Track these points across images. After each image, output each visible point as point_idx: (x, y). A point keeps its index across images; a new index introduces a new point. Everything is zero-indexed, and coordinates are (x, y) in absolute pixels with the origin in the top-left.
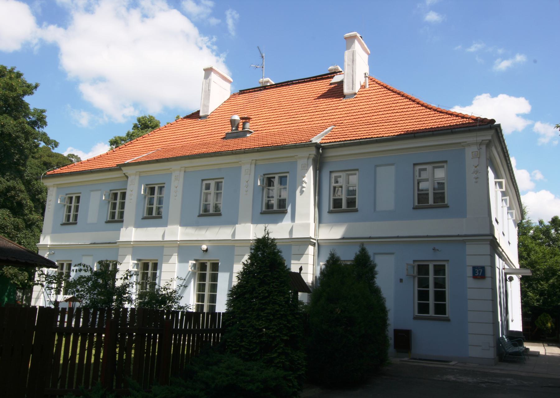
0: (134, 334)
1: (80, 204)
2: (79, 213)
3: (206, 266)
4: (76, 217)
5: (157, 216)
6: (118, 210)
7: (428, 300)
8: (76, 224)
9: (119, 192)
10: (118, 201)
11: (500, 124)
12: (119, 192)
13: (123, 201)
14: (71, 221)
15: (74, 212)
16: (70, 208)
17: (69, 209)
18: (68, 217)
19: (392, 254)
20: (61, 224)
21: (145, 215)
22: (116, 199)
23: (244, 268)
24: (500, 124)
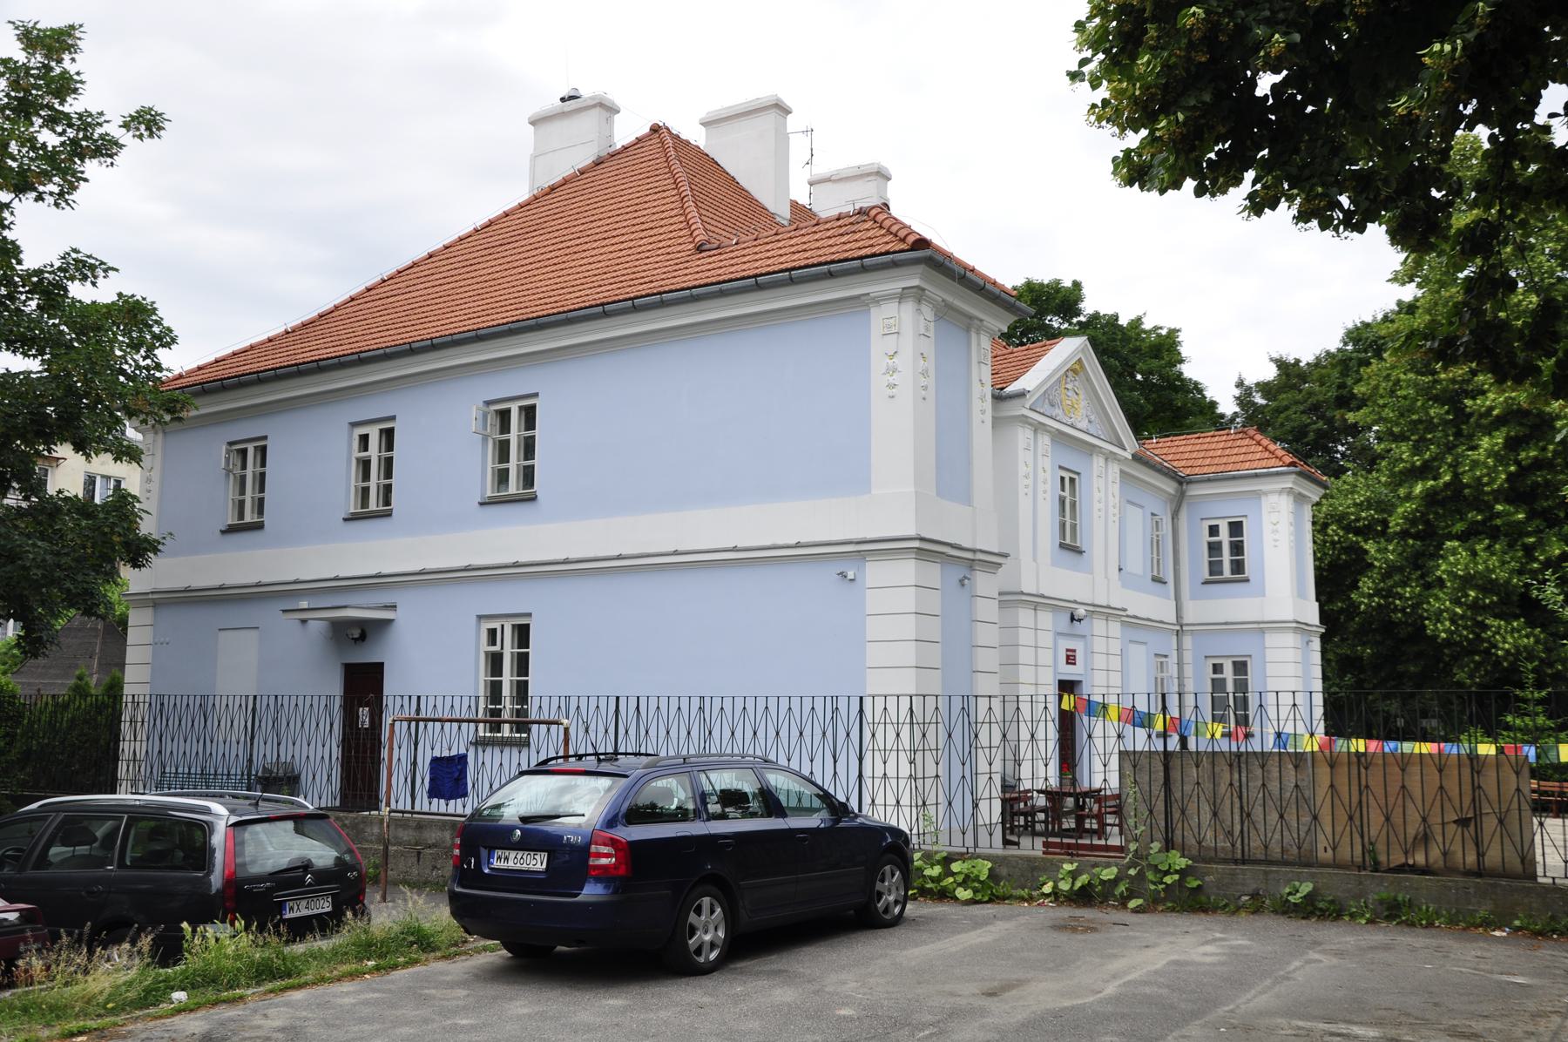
0: (1547, 29)
1: (395, 454)
2: (537, 462)
3: (449, 797)
4: (528, 476)
5: (381, 508)
6: (516, 463)
7: (1235, 680)
8: (388, 514)
9: (514, 409)
10: (515, 435)
11: (1173, 333)
12: (514, 409)
13: (530, 433)
14: (373, 506)
15: (253, 493)
16: (365, 465)
17: (503, 451)
18: (502, 477)
19: (1145, 643)
20: (345, 520)
21: (489, 494)
22: (505, 428)
23: (1180, 353)
24: (1173, 333)
